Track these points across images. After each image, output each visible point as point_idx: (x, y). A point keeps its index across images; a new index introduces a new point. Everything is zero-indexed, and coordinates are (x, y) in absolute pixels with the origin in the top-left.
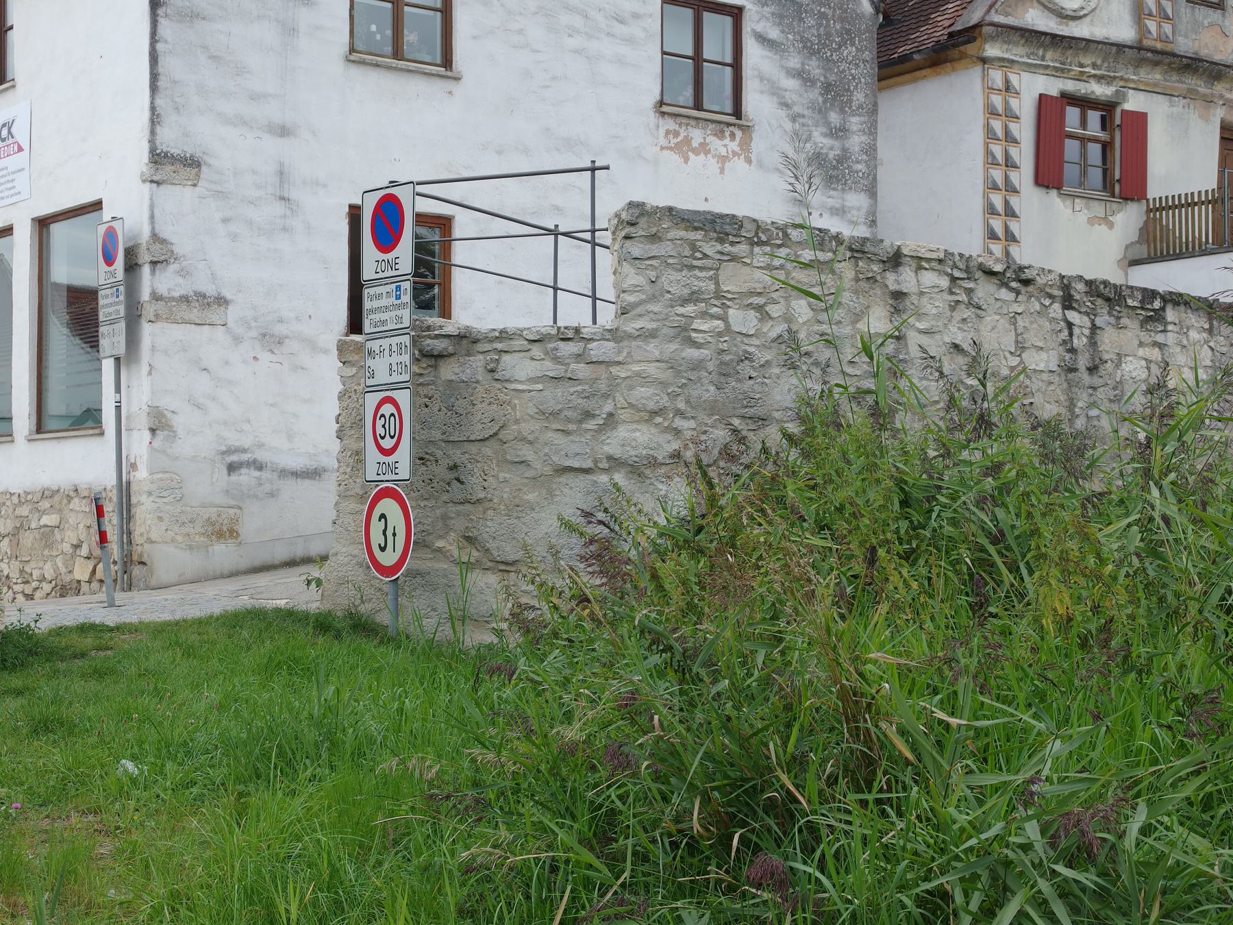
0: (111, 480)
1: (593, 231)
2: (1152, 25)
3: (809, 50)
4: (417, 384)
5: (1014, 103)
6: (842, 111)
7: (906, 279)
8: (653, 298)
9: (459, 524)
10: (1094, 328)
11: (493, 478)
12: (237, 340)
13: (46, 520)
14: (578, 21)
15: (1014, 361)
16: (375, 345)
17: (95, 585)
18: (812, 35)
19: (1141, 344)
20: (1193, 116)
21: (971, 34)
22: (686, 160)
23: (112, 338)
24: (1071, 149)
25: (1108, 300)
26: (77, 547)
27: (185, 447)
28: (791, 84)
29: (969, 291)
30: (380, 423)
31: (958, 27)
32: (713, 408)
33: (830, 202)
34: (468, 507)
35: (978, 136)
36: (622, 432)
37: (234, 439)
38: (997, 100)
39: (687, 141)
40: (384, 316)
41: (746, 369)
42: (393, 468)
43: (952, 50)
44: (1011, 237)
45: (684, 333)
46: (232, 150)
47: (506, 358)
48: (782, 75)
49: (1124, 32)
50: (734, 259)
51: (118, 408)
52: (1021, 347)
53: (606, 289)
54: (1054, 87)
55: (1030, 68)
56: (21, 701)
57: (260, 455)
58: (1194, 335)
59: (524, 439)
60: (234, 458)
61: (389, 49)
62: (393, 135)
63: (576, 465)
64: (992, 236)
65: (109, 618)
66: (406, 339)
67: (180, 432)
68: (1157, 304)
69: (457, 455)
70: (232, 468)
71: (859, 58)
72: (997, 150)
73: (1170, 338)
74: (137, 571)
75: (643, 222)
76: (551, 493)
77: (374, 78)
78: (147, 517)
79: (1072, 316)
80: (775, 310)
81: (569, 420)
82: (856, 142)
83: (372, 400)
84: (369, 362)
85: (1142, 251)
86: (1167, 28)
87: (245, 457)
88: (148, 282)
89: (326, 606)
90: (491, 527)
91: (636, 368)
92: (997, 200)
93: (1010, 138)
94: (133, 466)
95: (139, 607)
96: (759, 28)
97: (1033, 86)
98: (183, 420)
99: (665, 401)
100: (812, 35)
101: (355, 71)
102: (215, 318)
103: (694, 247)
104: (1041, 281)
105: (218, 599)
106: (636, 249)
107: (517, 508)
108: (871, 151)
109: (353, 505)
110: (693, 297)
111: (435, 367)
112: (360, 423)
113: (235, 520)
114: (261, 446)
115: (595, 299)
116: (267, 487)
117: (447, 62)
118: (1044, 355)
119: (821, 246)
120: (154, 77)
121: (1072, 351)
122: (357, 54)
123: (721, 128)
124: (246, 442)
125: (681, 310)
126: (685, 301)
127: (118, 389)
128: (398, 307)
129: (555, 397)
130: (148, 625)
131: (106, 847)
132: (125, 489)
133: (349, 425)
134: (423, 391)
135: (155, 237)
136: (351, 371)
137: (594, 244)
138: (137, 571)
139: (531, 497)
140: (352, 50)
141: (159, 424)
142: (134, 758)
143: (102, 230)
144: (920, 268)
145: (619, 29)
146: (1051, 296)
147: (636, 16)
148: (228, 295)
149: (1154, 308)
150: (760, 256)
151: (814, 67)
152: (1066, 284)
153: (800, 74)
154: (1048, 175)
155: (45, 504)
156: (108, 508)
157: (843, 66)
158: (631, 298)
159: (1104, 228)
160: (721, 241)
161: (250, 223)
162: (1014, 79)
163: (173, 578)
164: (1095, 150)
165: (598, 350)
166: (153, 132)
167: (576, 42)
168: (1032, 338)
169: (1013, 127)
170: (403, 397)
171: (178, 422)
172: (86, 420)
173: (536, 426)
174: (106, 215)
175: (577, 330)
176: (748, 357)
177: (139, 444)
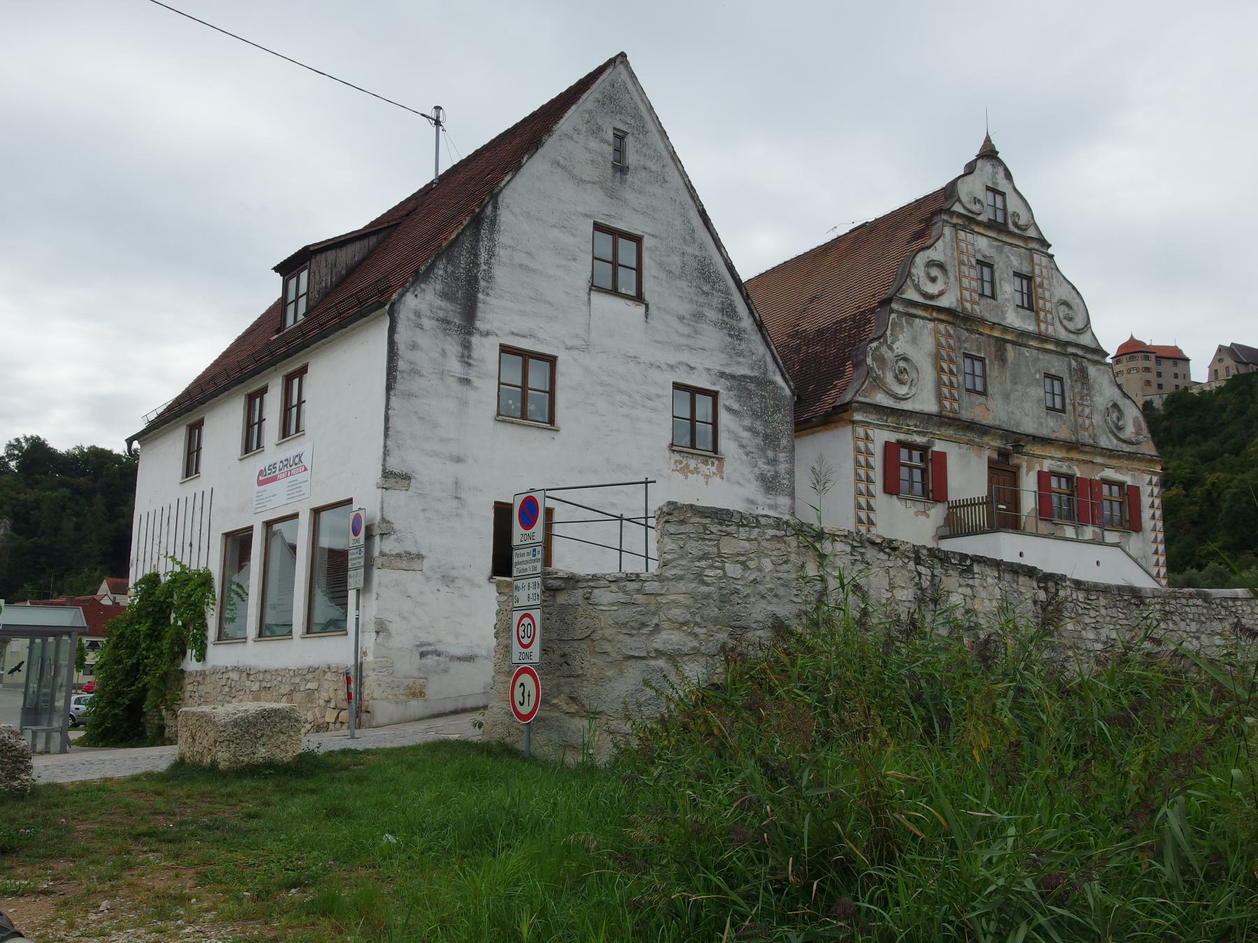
0: (353, 662)
1: (646, 518)
2: (947, 404)
3: (756, 415)
4: (544, 606)
5: (871, 446)
6: (775, 450)
7: (827, 547)
8: (681, 557)
9: (566, 689)
10: (933, 576)
11: (588, 663)
12: (428, 579)
13: (310, 686)
14: (626, 399)
15: (889, 595)
16: (519, 583)
17: (338, 725)
18: (757, 407)
19: (960, 586)
20: (972, 455)
21: (846, 407)
22: (687, 477)
23: (355, 579)
24: (904, 472)
25: (940, 559)
26: (328, 702)
27: (396, 642)
28: (746, 434)
29: (862, 554)
30: (521, 629)
31: (838, 403)
32: (716, 621)
33: (769, 501)
34: (572, 679)
35: (850, 465)
36: (664, 635)
37: (424, 637)
38: (861, 444)
39: (687, 466)
40: (525, 567)
41: (735, 598)
42: (529, 656)
43: (835, 416)
44: (871, 523)
45: (700, 578)
46: (429, 471)
47: (596, 591)
48: (741, 429)
49: (931, 407)
50: (728, 534)
51: (357, 619)
52: (892, 587)
53: (653, 553)
54: (893, 437)
55: (879, 426)
56: (315, 797)
57: (440, 647)
58: (990, 580)
59: (606, 639)
60: (424, 649)
61: (519, 414)
62: (516, 463)
63: (637, 654)
64: (860, 521)
65: (351, 744)
66: (539, 580)
67: (393, 633)
68: (968, 562)
69: (566, 648)
70: (423, 655)
71: (783, 421)
72: (862, 472)
73: (977, 582)
74: (364, 716)
75: (676, 513)
76: (621, 671)
77: (511, 429)
78: (372, 686)
79: (921, 569)
80: (752, 564)
81: (633, 628)
82: (783, 467)
83: (517, 616)
84: (516, 593)
85: (946, 531)
86: (956, 405)
87: (430, 648)
88: (377, 543)
89: (485, 739)
90: (585, 690)
91: (672, 597)
92: (863, 501)
93: (869, 466)
94: (365, 654)
95: (367, 740)
96: (727, 403)
97: (881, 437)
98: (395, 626)
99: (689, 617)
100: (757, 407)
101: (500, 426)
102: (416, 567)
103: (705, 528)
104: (902, 548)
105: (414, 735)
106: (672, 528)
107: (601, 680)
108: (791, 473)
109: (503, 678)
110: (705, 557)
111: (554, 596)
112: (509, 629)
113: (423, 686)
114: (440, 641)
115: (647, 557)
116: (442, 667)
117: (552, 420)
118: (906, 592)
119: (778, 527)
120: (387, 429)
121: (921, 589)
122: (502, 416)
123: (706, 459)
124: (431, 639)
125: (698, 564)
126: (700, 559)
127: (358, 608)
128: (534, 561)
129: (624, 614)
130: (383, 750)
131: (387, 889)
132: (359, 667)
133: (502, 630)
134: (547, 610)
135: (383, 519)
136: (504, 598)
137: (647, 526)
138: (364, 716)
139: (609, 673)
140: (499, 414)
141: (381, 629)
142: (392, 833)
143: (352, 515)
144: (834, 540)
145: (649, 403)
146: (908, 557)
147: (658, 396)
148: (423, 552)
149: (967, 564)
150: (743, 532)
151: (758, 425)
152: (916, 550)
153: (750, 429)
154: (891, 488)
155: (310, 676)
156: (353, 679)
157: (775, 425)
158: (669, 557)
159: (924, 517)
160: (721, 524)
161: (437, 511)
162: (870, 433)
163: (385, 721)
164: (917, 475)
165: (651, 587)
166: (385, 460)
167: (624, 410)
168: (899, 581)
169: (871, 459)
170: (537, 614)
171: (392, 627)
172: (336, 626)
173: (613, 631)
174: (355, 507)
175: (638, 575)
176: (736, 592)
177: (369, 640)
